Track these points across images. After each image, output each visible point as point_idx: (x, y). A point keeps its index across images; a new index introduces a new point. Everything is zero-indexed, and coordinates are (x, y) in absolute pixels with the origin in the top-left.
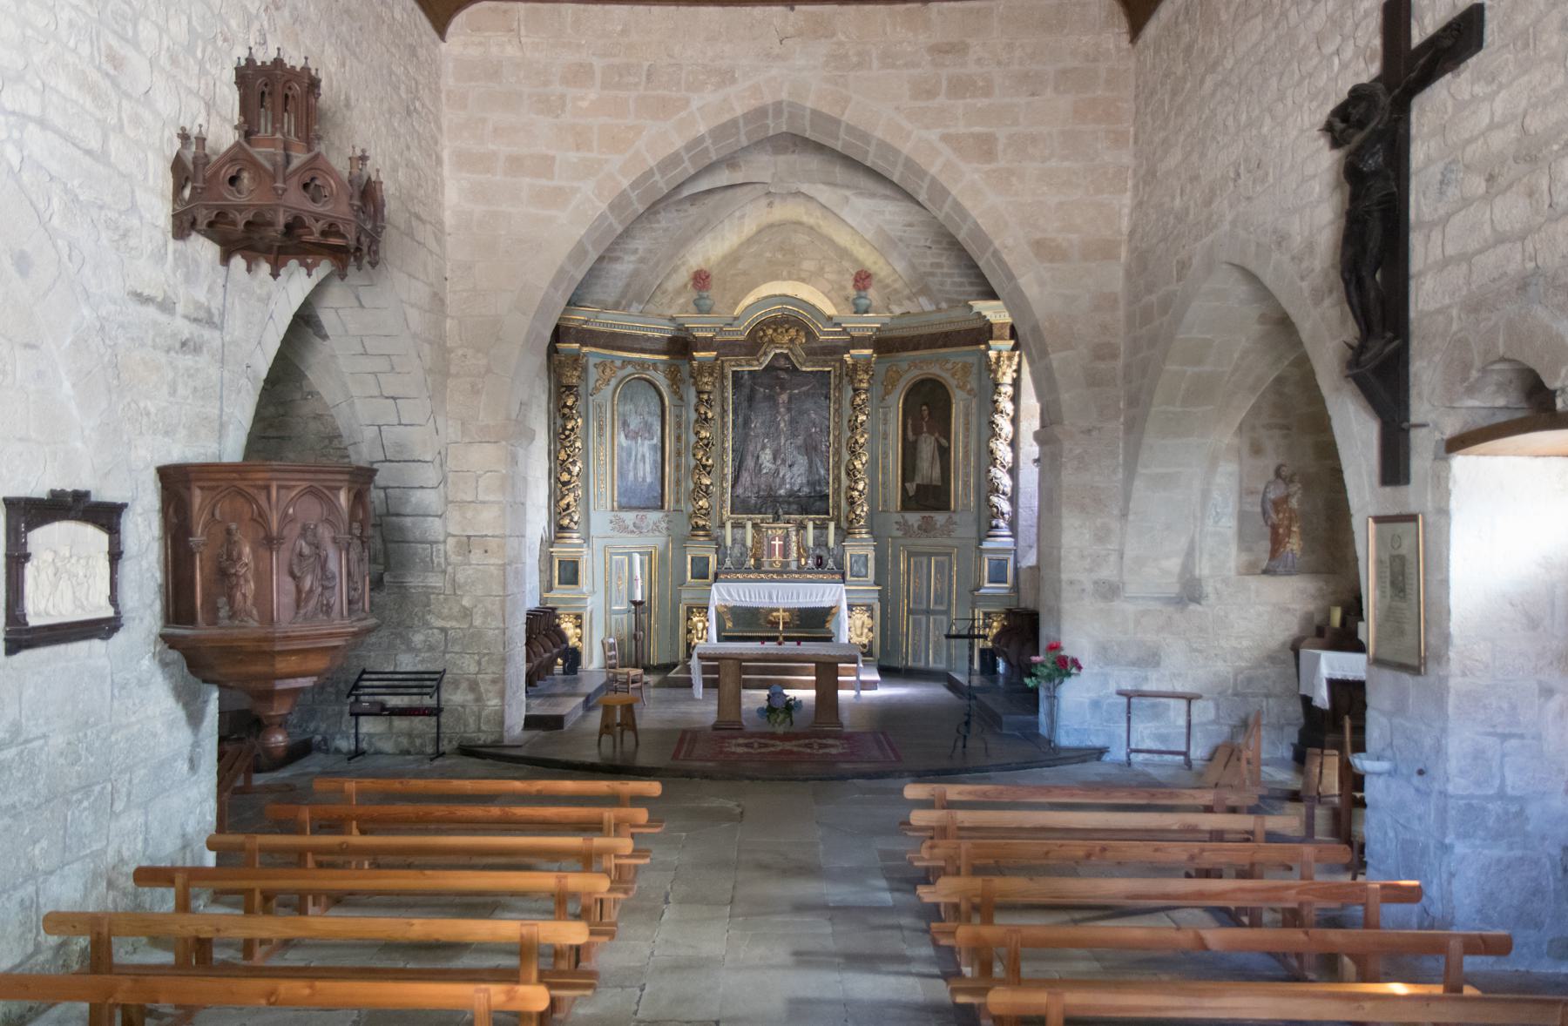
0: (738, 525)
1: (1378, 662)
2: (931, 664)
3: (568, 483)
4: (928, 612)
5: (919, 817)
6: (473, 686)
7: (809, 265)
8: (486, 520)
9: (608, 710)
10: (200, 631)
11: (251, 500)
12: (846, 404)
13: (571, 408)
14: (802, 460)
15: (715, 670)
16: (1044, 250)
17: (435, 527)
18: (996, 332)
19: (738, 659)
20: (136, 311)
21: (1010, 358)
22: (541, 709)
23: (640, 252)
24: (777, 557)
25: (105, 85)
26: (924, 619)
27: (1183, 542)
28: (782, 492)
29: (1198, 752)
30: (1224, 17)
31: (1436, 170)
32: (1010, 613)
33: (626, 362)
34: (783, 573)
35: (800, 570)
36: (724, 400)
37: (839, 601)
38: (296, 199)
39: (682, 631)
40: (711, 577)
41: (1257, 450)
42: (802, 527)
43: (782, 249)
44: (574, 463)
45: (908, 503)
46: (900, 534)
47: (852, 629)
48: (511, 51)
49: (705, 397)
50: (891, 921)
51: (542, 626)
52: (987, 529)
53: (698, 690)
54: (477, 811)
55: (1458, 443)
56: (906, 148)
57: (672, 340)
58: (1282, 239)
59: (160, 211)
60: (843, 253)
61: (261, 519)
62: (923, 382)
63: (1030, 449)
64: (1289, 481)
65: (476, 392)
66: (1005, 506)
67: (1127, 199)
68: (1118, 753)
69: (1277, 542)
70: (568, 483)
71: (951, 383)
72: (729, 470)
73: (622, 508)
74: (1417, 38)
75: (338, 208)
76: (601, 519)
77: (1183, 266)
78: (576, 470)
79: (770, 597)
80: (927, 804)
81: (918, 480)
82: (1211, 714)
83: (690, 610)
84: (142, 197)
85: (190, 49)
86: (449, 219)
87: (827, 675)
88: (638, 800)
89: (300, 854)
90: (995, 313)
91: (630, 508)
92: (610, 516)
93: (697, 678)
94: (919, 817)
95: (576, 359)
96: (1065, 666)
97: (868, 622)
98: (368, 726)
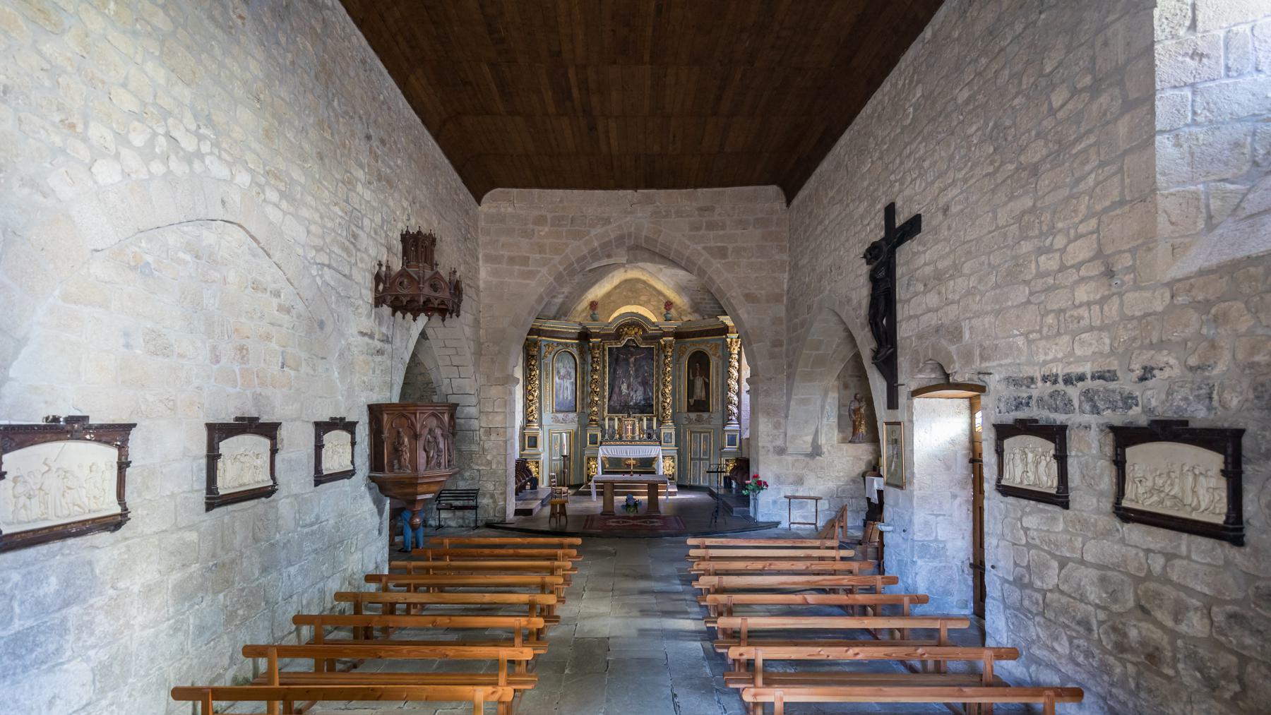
0: (611, 419)
1: (887, 484)
4: (700, 459)
5: (693, 552)
6: (492, 496)
7: (643, 298)
8: (497, 421)
9: (554, 506)
10: (387, 474)
11: (408, 418)
14: (641, 389)
15: (602, 487)
16: (750, 298)
17: (475, 424)
19: (612, 483)
20: (360, 338)
22: (522, 506)
24: (630, 434)
25: (351, 247)
27: (813, 429)
29: (820, 524)
30: (825, 202)
31: (906, 278)
32: (737, 460)
33: (559, 344)
34: (632, 441)
36: (604, 361)
38: (427, 291)
41: (846, 387)
42: (641, 420)
47: (665, 467)
48: (510, 210)
50: (682, 597)
51: (522, 468)
52: (726, 420)
53: (594, 496)
54: (503, 551)
55: (916, 393)
56: (687, 253)
58: (849, 301)
59: (369, 296)
60: (660, 293)
61: (412, 427)
63: (746, 387)
64: (859, 401)
65: (493, 362)
66: (735, 410)
67: (786, 275)
68: (785, 525)
69: (855, 429)
72: (607, 394)
74: (897, 225)
75: (445, 294)
76: (547, 417)
77: (810, 308)
80: (697, 547)
82: (827, 506)
84: (364, 291)
85: (382, 227)
86: (481, 285)
87: (653, 489)
88: (571, 546)
89: (427, 569)
90: (727, 320)
93: (593, 490)
94: (693, 552)
96: (761, 485)
98: (444, 515)
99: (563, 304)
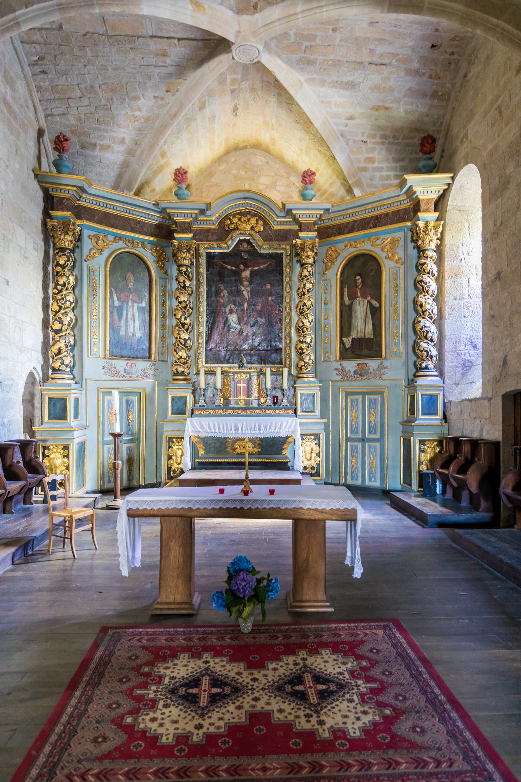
2: (367, 483)
3: (61, 330)
4: (363, 440)
12: (296, 278)
13: (63, 267)
18: (423, 206)
21: (436, 227)
23: (127, 141)
24: (242, 397)
26: (360, 445)
28: (246, 347)
34: (246, 410)
35: (260, 407)
36: (199, 274)
37: (294, 431)
39: (164, 457)
40: (188, 412)
43: (244, 167)
44: (66, 314)
45: (346, 354)
46: (339, 378)
47: (304, 454)
49: (184, 269)
57: (158, 227)
62: (356, 257)
70: (61, 330)
71: (381, 255)
73: (113, 356)
76: (94, 364)
78: (66, 320)
79: (236, 429)
81: (354, 335)
83: (170, 440)
91: (122, 357)
92: (103, 362)
95: (66, 226)
97: (316, 449)
99: (125, 165)
